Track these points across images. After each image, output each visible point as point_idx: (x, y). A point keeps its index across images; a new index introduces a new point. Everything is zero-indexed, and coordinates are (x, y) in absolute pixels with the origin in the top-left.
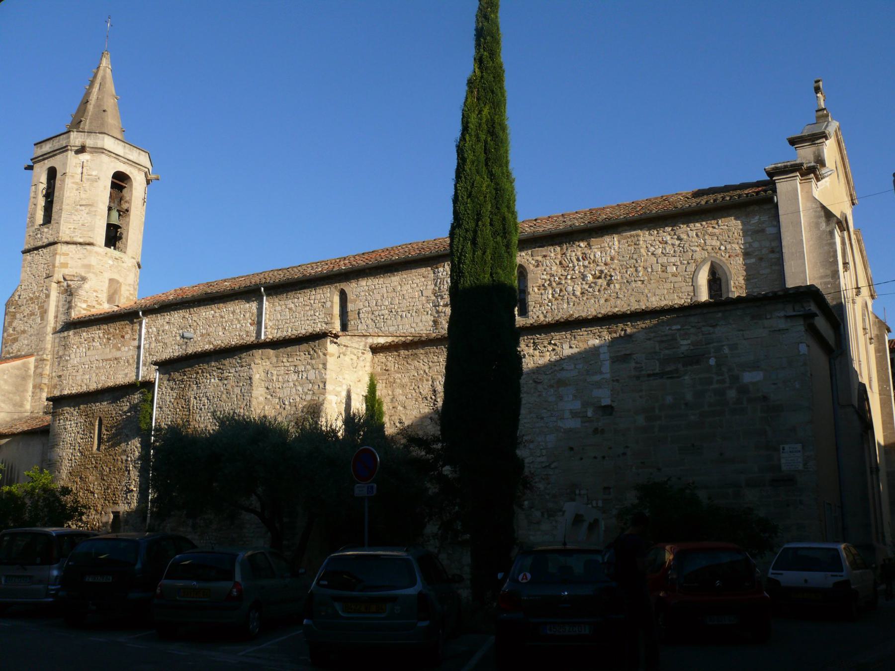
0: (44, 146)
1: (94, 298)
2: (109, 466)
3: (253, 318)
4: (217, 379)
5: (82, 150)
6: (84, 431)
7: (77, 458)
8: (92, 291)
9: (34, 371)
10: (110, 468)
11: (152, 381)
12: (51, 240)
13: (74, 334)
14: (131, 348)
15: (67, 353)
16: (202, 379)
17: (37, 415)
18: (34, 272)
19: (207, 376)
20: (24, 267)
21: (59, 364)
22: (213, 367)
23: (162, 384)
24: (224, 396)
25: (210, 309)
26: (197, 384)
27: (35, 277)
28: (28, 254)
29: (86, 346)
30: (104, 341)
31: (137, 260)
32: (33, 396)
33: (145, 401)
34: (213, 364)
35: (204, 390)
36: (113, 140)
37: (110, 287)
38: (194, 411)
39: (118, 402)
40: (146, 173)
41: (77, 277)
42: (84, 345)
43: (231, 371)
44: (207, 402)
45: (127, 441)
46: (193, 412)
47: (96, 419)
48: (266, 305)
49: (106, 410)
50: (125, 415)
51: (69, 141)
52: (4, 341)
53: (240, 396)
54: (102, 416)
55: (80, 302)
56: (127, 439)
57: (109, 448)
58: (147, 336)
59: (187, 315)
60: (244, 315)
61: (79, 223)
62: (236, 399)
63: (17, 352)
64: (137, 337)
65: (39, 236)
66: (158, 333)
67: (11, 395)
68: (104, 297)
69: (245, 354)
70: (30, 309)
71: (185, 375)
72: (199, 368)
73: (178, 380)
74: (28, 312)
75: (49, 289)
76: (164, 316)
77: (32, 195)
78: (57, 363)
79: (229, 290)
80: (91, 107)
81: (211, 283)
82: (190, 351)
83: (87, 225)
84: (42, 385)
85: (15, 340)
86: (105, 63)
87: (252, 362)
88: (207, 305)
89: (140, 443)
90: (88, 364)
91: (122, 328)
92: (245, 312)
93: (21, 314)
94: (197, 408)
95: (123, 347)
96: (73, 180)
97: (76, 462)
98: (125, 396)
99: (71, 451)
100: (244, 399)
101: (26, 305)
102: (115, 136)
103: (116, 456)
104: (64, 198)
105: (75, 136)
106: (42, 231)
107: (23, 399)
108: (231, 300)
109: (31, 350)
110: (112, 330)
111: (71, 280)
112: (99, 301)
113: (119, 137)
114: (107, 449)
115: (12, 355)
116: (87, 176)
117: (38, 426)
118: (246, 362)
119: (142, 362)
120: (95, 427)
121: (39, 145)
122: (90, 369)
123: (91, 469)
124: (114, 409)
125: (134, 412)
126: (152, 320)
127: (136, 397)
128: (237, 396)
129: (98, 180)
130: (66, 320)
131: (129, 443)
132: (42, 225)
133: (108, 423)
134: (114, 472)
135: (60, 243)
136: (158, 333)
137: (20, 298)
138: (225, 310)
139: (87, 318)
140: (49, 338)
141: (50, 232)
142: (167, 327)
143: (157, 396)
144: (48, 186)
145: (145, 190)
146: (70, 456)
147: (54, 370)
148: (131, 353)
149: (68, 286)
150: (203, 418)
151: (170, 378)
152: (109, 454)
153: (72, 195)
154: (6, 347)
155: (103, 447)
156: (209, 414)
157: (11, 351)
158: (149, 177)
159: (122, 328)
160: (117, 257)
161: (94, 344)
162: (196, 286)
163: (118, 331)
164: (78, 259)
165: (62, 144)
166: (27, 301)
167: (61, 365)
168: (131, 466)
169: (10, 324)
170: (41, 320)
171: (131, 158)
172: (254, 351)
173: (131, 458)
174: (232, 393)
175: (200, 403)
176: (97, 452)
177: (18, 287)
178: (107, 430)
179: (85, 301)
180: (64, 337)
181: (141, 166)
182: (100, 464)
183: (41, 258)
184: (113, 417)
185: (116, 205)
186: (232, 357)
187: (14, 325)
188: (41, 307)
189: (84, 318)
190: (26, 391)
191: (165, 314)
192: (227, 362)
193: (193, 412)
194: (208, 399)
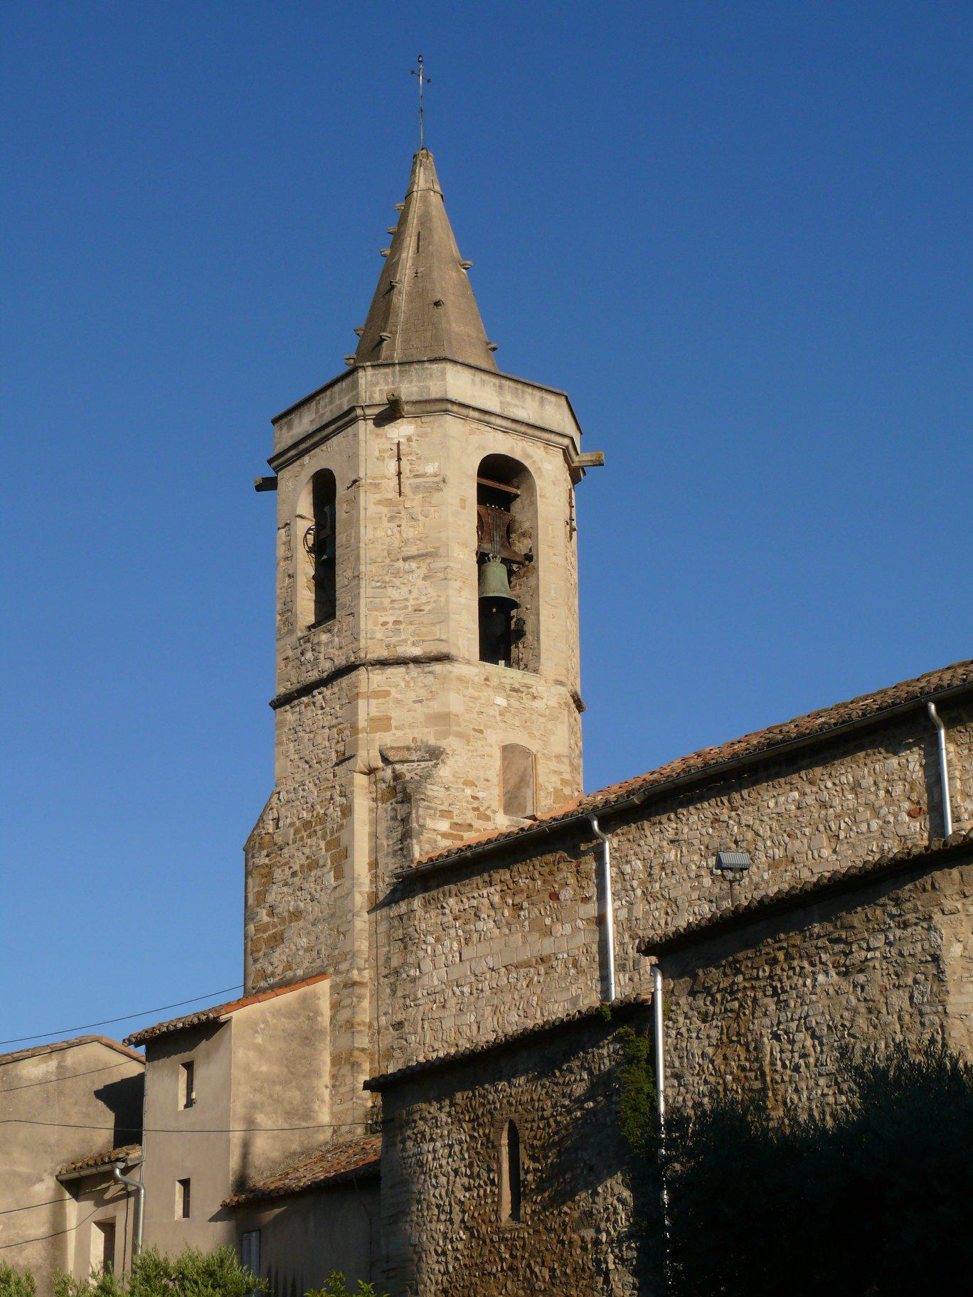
0: (296, 421)
1: (468, 802)
2: (548, 1262)
3: (914, 797)
4: (832, 972)
5: (391, 412)
6: (471, 1165)
7: (460, 1246)
8: (461, 786)
9: (333, 1018)
10: (552, 1270)
11: (645, 1001)
12: (341, 661)
13: (425, 906)
14: (579, 923)
15: (411, 959)
16: (789, 978)
17: (349, 1137)
18: (305, 753)
19: (802, 968)
20: (281, 743)
21: (394, 992)
22: (819, 937)
23: (673, 1008)
24: (861, 1022)
25: (788, 787)
26: (775, 993)
27: (310, 767)
28: (288, 707)
29: (460, 932)
30: (506, 913)
31: (571, 687)
32: (334, 1086)
33: (631, 1060)
34: (817, 928)
35: (798, 1011)
36: (466, 375)
37: (506, 768)
38: (778, 1077)
39: (558, 1074)
40: (565, 452)
41: (416, 750)
42: (452, 932)
43: (874, 943)
44: (814, 1046)
45: (592, 1187)
46: (772, 1080)
47: (502, 1129)
48: (948, 753)
49: (524, 1099)
50: (582, 1108)
51: (357, 397)
52: (249, 946)
53: (911, 1015)
54: (514, 1116)
55: (433, 817)
56: (592, 1179)
57: (545, 1209)
58: (619, 886)
59: (725, 814)
60: (887, 791)
61: (406, 607)
62: (898, 1027)
63: (283, 971)
64: (592, 891)
65: (309, 655)
66: (650, 875)
67: (278, 1088)
68: (492, 796)
69: (910, 886)
70: (307, 851)
71: (738, 972)
72: (777, 946)
73: (719, 991)
74: (303, 861)
75: (348, 791)
76: (660, 823)
77: (281, 551)
78: (388, 990)
79: (835, 724)
80: (401, 301)
81: (781, 726)
82: (745, 895)
83: (427, 608)
84: (356, 1053)
85: (278, 939)
86: (424, 179)
87: (936, 910)
88: (778, 775)
89: (627, 1186)
90: (471, 984)
91: (551, 873)
92: (888, 781)
93: (286, 868)
94: (784, 1066)
95: (559, 926)
96: (378, 496)
97: (457, 1259)
98: (575, 1054)
99: (442, 1228)
100: (922, 1024)
101: (294, 842)
102: (473, 365)
103: (565, 1231)
104: (362, 545)
105: (369, 378)
106: (316, 641)
107: (309, 1096)
108: (845, 755)
109: (319, 963)
110: (523, 882)
111: (403, 762)
112: (482, 809)
113: (484, 366)
114: (540, 1213)
115: (272, 981)
116: (413, 481)
117: (353, 1167)
118: (916, 910)
119: (615, 960)
120: (499, 1152)
121: (285, 420)
122: (475, 995)
123: (499, 1275)
124: (547, 1093)
125: (605, 1096)
126: (629, 840)
127: (605, 1052)
128: (900, 1018)
129: (441, 485)
130: (399, 871)
131: (600, 1190)
132: (313, 626)
133: (535, 1138)
134: (563, 1279)
135: (363, 665)
136: (650, 875)
137: (278, 827)
138: (829, 785)
139: (453, 857)
140: (362, 922)
141: (336, 640)
142: (672, 855)
143: (665, 1044)
144: (317, 524)
145: (570, 497)
146: (441, 1243)
147: (382, 1010)
148: (581, 939)
149: (397, 777)
150: (805, 1094)
151: (696, 988)
152: (546, 1228)
153: (380, 534)
154: (256, 961)
155: (526, 1209)
156: (822, 1081)
157: (270, 969)
158: (577, 461)
159: (551, 873)
160: (517, 686)
161: (480, 925)
162: (739, 742)
163: (539, 882)
164: (415, 702)
165: (340, 406)
166: (296, 832)
167: (399, 994)
168: (611, 1258)
169: (261, 897)
170: (336, 878)
171: (521, 414)
172: (937, 874)
173: (608, 1233)
174: (884, 1011)
175: (792, 1051)
176: (513, 1224)
177: (271, 798)
178: (534, 1158)
179: (446, 814)
180: (400, 917)
181: (551, 432)
182: (523, 1258)
183: (320, 712)
184: (547, 1119)
185: (498, 547)
186: (871, 901)
187: (270, 899)
188: (333, 844)
189: (447, 856)
190: (315, 1073)
191: (664, 818)
192: (857, 918)
193: (772, 1080)
194: (813, 1036)
